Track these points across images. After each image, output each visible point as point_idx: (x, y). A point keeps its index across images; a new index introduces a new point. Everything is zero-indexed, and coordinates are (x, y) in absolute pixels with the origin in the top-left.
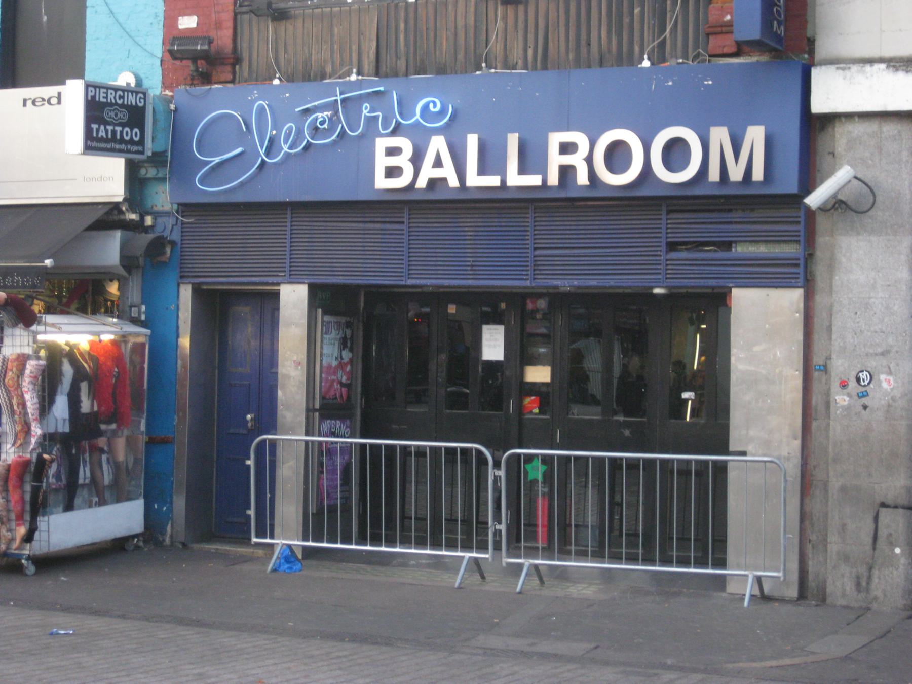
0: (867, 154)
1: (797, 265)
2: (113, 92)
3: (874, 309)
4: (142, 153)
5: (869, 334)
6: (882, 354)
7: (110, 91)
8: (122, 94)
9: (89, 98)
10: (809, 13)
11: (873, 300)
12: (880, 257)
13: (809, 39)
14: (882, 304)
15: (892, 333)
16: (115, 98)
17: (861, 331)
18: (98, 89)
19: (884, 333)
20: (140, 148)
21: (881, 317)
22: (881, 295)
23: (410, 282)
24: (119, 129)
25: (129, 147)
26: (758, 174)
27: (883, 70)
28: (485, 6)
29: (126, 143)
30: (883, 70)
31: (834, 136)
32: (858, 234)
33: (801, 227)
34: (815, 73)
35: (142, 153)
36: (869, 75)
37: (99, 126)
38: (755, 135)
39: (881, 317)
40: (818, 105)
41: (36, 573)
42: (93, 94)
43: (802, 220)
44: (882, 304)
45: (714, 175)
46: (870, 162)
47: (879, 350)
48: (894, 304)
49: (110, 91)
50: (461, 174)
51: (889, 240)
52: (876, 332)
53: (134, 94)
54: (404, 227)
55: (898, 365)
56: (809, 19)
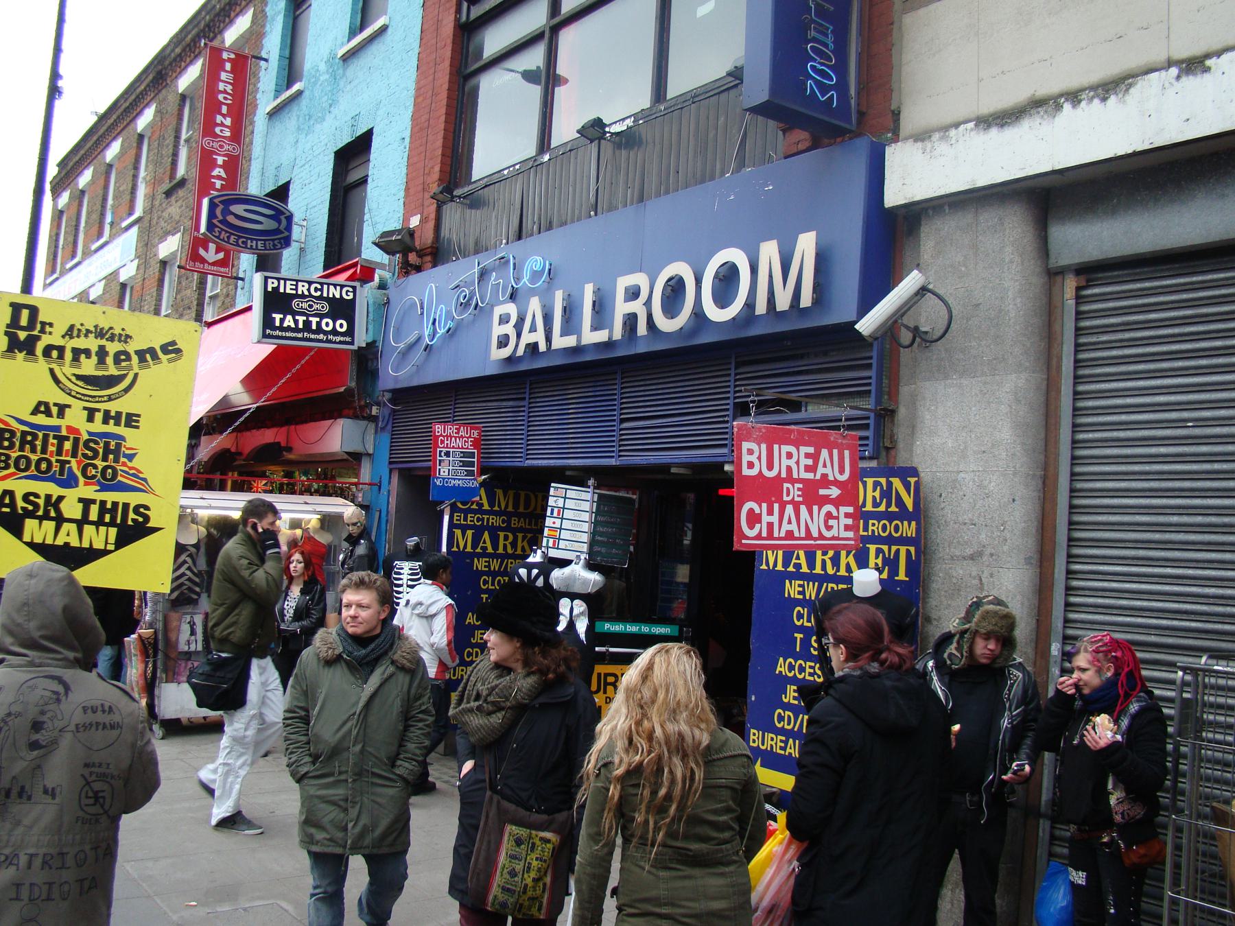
0: (960, 258)
1: (866, 427)
2: (306, 285)
3: (964, 489)
4: (352, 343)
5: (956, 526)
6: (972, 558)
7: (300, 284)
8: (319, 287)
9: (270, 289)
10: (894, 78)
11: (962, 475)
12: (973, 409)
13: (893, 112)
14: (974, 481)
15: (986, 526)
16: (309, 290)
17: (945, 522)
18: (282, 282)
19: (975, 525)
20: (348, 339)
21: (971, 500)
22: (973, 467)
23: (529, 463)
24: (314, 320)
25: (330, 337)
26: (806, 300)
27: (972, 130)
28: (594, 155)
29: (325, 333)
30: (972, 130)
31: (919, 237)
32: (946, 377)
33: (872, 373)
34: (890, 152)
35: (352, 343)
36: (953, 142)
37: (285, 317)
38: (806, 244)
39: (971, 500)
40: (893, 197)
41: (1057, 688)
42: (276, 285)
43: (874, 362)
44: (974, 481)
45: (761, 308)
46: (963, 269)
47: (969, 551)
48: (990, 482)
49: (300, 284)
50: (549, 339)
51: (985, 383)
52: (965, 524)
53: (338, 288)
54: (525, 403)
55: (991, 575)
56: (894, 86)
